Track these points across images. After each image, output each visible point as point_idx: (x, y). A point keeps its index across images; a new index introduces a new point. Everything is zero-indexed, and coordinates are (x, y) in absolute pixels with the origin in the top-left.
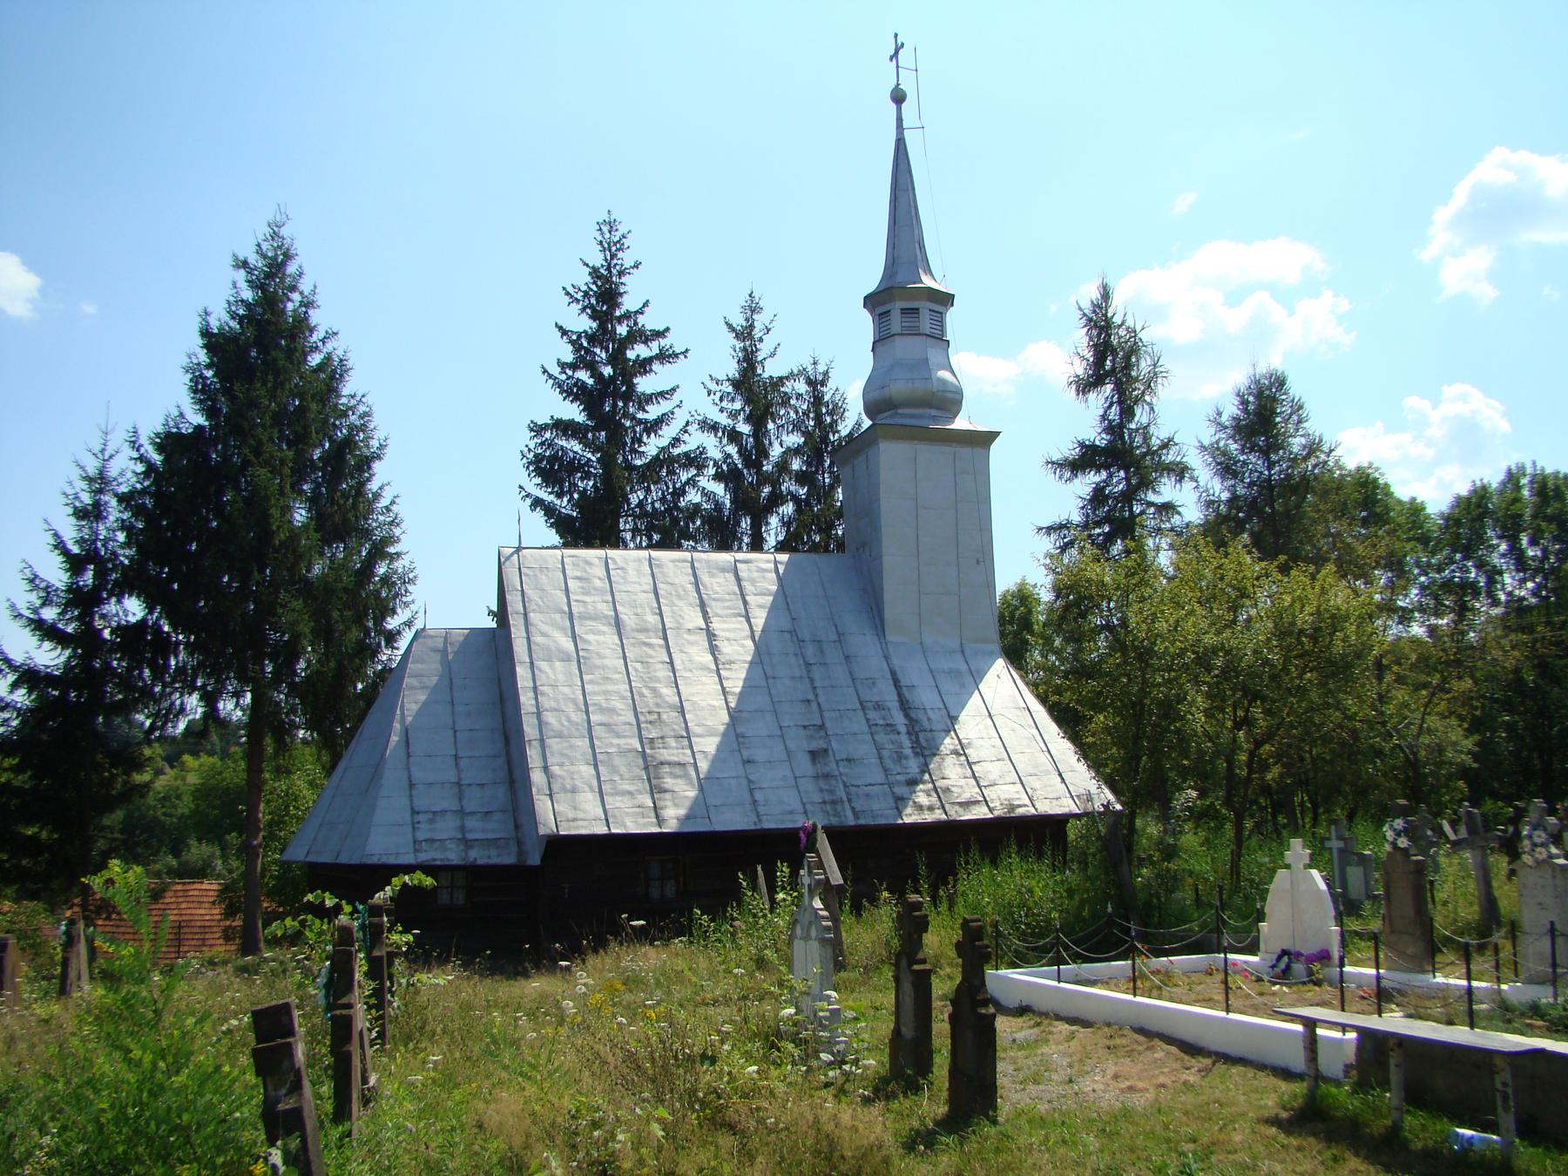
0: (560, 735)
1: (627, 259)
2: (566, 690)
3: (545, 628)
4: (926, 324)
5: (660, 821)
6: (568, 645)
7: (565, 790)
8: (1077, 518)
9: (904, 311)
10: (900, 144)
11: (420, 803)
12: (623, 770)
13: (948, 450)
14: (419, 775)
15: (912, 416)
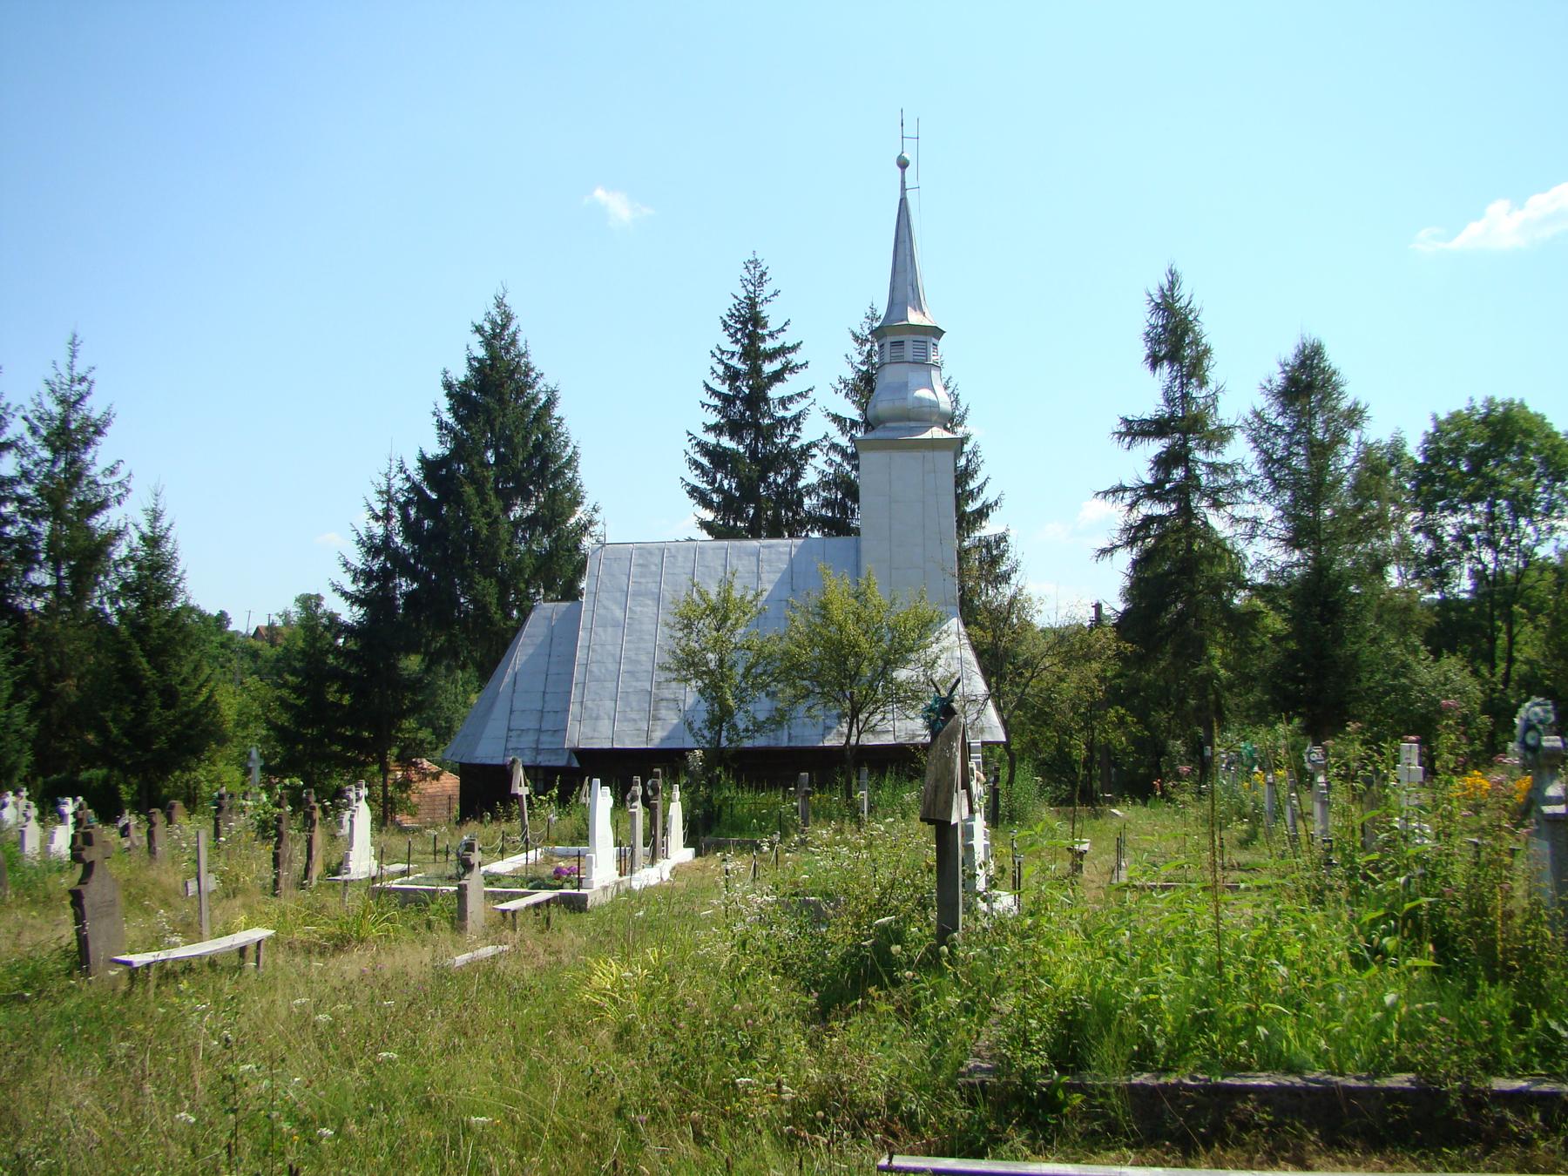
0: (598, 680)
1: (767, 290)
2: (609, 648)
3: (606, 603)
4: (909, 353)
5: (648, 739)
6: (619, 614)
7: (591, 717)
8: (1148, 480)
9: (894, 344)
10: (903, 202)
11: (514, 725)
12: (634, 704)
13: (918, 454)
14: (518, 705)
15: (893, 429)
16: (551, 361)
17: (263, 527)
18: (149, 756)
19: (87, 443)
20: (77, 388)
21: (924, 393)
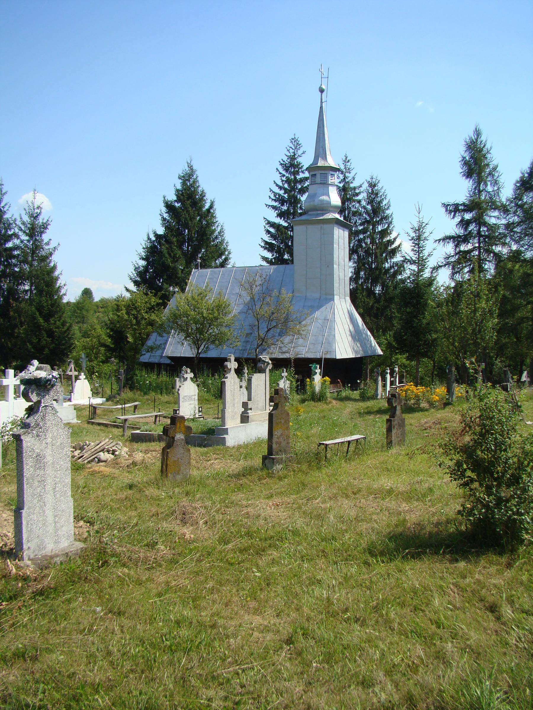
1: (300, 152)
4: (318, 179)
10: (321, 108)
13: (319, 226)
16: (211, 189)
17: (97, 263)
18: (43, 356)
19: (42, 233)
20: (36, 211)
21: (325, 198)
